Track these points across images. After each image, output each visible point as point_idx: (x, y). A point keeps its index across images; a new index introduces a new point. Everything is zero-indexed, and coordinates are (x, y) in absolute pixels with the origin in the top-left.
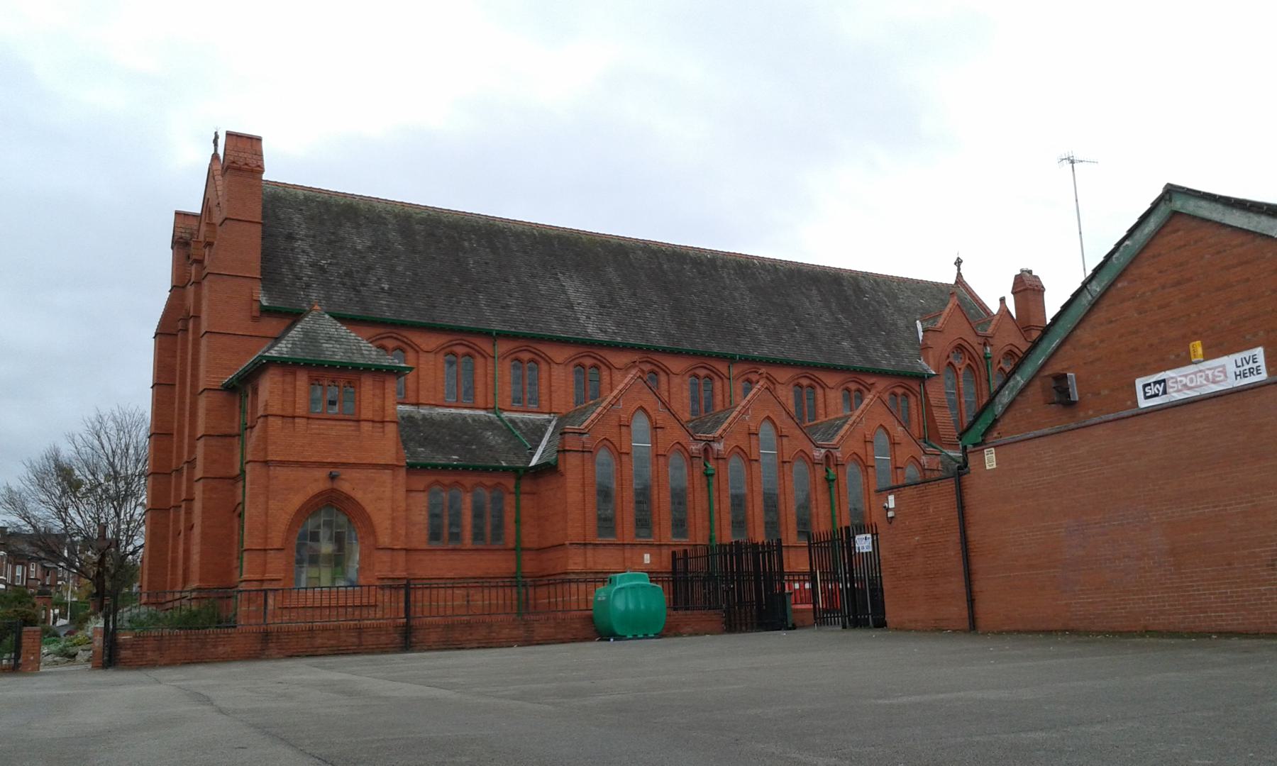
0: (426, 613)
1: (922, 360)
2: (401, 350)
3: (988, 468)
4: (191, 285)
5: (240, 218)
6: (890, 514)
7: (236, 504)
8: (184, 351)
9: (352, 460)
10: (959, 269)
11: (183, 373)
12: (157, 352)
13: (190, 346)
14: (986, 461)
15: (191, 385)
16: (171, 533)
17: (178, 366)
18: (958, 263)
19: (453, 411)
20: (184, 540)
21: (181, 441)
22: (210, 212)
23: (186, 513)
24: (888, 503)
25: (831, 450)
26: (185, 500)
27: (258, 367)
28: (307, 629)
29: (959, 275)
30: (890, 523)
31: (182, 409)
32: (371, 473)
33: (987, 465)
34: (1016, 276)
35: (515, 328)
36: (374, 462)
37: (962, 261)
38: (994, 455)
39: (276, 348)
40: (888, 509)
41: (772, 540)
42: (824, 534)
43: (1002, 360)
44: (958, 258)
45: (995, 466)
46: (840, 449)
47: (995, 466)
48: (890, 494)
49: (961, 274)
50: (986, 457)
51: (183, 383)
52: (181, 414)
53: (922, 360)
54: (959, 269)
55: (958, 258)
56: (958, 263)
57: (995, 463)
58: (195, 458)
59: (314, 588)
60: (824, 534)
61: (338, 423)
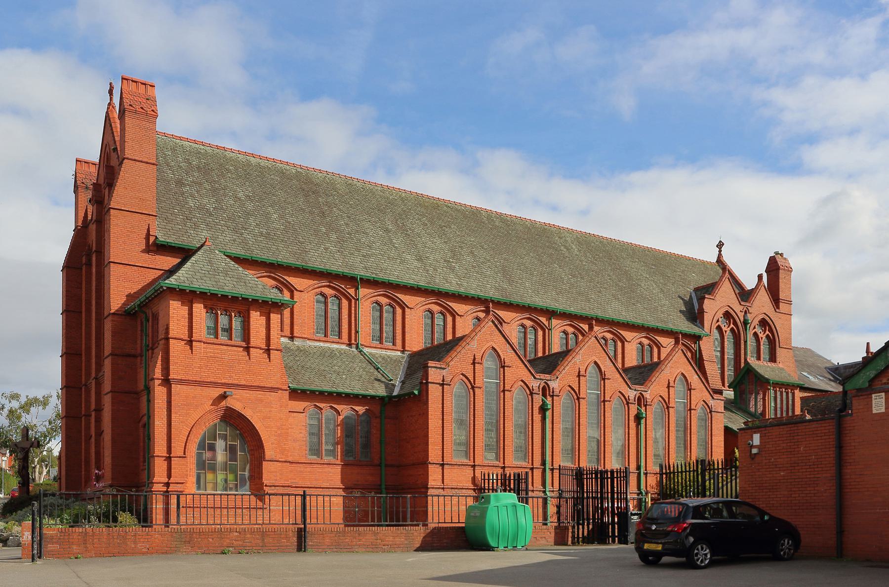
0: (320, 521)
1: (698, 322)
2: (279, 289)
3: (874, 411)
4: (93, 224)
5: (137, 158)
6: (754, 451)
7: (141, 416)
8: (89, 282)
9: (243, 382)
10: (720, 251)
11: (89, 303)
12: (64, 284)
13: (94, 278)
14: (874, 405)
15: (96, 312)
16: (83, 438)
17: (84, 295)
18: (720, 245)
19: (322, 344)
20: (95, 444)
21: (89, 360)
22: (108, 159)
23: (96, 421)
24: (752, 441)
25: (643, 393)
26: (84, 415)
27: (158, 294)
28: (210, 531)
29: (720, 255)
30: (753, 459)
31: (88, 334)
32: (259, 394)
33: (874, 409)
34: (770, 257)
35: (376, 274)
36: (262, 384)
37: (723, 244)
38: (883, 400)
39: (174, 277)
40: (752, 447)
41: (522, 473)
42: (718, 463)
43: (756, 326)
44: (720, 242)
45: (883, 410)
46: (649, 392)
47: (883, 410)
48: (755, 433)
49: (721, 255)
50: (874, 402)
51: (89, 311)
52: (88, 337)
53: (698, 322)
54: (720, 251)
55: (720, 242)
56: (720, 245)
57: (884, 407)
58: (104, 375)
59: (324, 496)
60: (718, 463)
61: (230, 348)
